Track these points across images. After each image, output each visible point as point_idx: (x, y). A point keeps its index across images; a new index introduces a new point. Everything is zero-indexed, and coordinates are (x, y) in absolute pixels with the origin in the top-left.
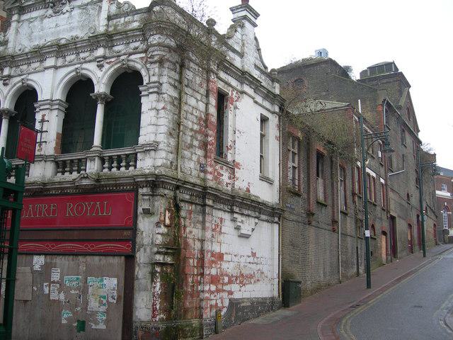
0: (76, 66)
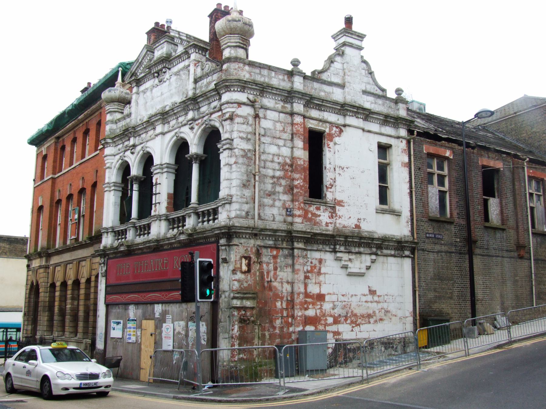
0: (175, 131)
